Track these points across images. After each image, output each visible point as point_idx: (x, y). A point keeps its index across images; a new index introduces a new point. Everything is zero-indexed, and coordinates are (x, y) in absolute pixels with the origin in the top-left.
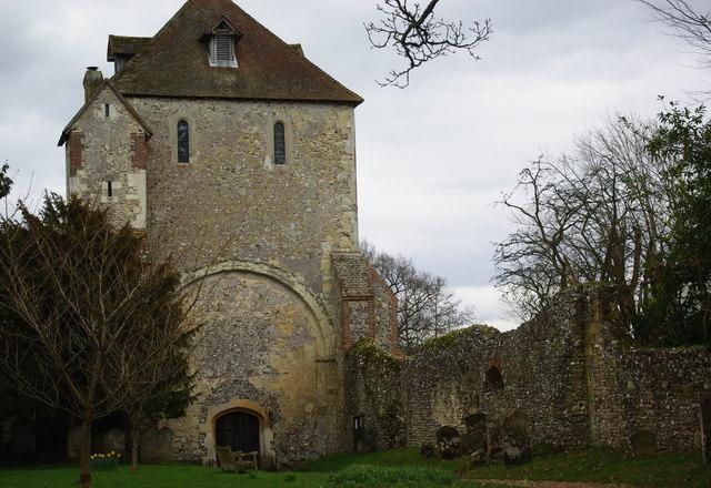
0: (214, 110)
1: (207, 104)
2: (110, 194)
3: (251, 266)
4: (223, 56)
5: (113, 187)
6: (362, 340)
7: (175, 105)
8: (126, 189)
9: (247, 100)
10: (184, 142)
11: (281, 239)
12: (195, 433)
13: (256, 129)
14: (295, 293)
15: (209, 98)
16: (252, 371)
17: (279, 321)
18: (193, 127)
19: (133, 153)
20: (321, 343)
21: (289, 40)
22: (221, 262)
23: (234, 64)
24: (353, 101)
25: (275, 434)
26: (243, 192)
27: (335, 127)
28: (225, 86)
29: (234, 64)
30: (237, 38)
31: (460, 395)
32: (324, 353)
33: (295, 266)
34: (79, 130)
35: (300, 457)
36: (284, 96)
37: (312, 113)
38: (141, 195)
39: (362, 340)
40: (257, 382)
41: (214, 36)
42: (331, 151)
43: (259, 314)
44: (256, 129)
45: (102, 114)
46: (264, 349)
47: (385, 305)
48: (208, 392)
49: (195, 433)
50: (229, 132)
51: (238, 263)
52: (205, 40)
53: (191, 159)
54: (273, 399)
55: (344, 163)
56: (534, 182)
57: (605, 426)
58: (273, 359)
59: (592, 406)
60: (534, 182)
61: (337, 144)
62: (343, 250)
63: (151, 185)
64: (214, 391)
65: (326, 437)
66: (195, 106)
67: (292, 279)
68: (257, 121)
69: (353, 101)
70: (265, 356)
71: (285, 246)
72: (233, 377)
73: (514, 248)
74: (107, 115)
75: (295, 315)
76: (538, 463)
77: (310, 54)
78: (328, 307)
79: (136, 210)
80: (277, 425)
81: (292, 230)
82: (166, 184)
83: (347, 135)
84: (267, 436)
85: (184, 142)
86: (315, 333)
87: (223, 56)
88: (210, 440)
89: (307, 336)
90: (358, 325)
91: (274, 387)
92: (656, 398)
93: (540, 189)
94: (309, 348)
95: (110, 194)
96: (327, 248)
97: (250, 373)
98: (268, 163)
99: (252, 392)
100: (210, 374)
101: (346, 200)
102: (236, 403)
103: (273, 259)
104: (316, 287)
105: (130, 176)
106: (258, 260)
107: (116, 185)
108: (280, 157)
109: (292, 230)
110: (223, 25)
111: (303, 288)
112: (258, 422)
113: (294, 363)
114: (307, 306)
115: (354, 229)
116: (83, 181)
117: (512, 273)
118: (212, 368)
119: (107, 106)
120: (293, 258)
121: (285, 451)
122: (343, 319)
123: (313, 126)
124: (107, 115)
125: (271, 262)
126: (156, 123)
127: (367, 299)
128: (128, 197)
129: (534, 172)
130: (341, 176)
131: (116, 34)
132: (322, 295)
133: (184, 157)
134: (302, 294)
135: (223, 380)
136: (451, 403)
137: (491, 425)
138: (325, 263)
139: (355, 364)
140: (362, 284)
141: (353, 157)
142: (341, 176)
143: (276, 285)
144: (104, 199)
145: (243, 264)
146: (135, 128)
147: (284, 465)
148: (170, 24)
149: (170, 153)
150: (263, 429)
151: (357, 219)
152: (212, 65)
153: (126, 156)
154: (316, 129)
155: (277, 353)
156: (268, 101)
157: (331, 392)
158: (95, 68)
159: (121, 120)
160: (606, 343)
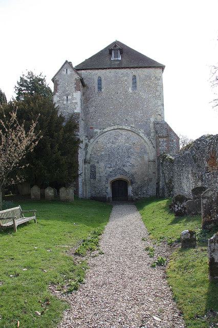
3: (124, 127)
4: (116, 56)
6: (164, 153)
7: (96, 71)
9: (122, 68)
11: (135, 117)
12: (104, 187)
13: (125, 78)
18: (103, 79)
20: (152, 155)
23: (120, 59)
29: (120, 59)
31: (194, 174)
32: (152, 158)
33: (141, 127)
34: (57, 79)
35: (142, 196)
39: (164, 153)
40: (126, 169)
42: (154, 85)
44: (125, 78)
45: (65, 73)
47: (174, 141)
55: (159, 88)
63: (86, 100)
64: (111, 172)
66: (104, 71)
67: (139, 131)
68: (126, 74)
69: (162, 67)
79: (76, 106)
81: (139, 114)
84: (130, 189)
88: (109, 190)
89: (145, 152)
90: (163, 147)
91: (133, 171)
96: (152, 120)
97: (124, 166)
98: (130, 90)
100: (109, 166)
102: (118, 177)
104: (148, 134)
107: (69, 97)
109: (139, 114)
110: (115, 46)
114: (145, 142)
116: (58, 96)
121: (137, 195)
122: (157, 146)
130: (157, 94)
133: (100, 88)
136: (189, 178)
137: (204, 201)
138: (152, 125)
141: (162, 87)
144: (65, 102)
146: (76, 76)
153: (73, 86)
154: (148, 77)
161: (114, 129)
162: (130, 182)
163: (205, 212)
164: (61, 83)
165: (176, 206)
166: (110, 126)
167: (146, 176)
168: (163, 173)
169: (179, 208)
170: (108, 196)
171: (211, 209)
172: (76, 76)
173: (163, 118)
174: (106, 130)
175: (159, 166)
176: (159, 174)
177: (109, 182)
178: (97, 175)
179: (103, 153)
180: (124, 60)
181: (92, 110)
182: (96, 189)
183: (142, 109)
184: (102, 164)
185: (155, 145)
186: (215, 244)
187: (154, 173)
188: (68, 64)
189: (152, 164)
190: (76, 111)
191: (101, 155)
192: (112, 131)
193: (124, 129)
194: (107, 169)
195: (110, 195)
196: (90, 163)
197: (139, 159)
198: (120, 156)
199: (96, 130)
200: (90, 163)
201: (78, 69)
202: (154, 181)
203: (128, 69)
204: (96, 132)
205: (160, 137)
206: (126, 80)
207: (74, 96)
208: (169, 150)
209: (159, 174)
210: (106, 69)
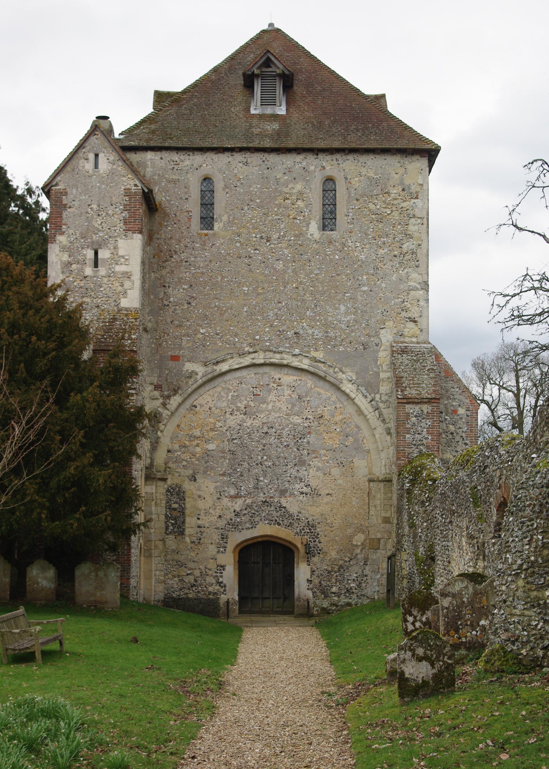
0: (246, 164)
1: (239, 156)
2: (96, 265)
3: (288, 359)
5: (100, 256)
7: (198, 158)
8: (116, 259)
10: (207, 205)
11: (326, 325)
12: (212, 565)
13: (299, 187)
14: (344, 392)
15: (241, 150)
16: (286, 491)
17: (322, 428)
18: (219, 186)
19: (125, 214)
20: (379, 458)
21: (368, 88)
22: (250, 353)
23: (282, 110)
25: (313, 572)
26: (280, 266)
27: (402, 183)
28: (262, 136)
29: (282, 110)
30: (288, 82)
32: (380, 471)
34: (61, 187)
35: (344, 600)
36: (336, 144)
37: (373, 165)
38: (134, 267)
40: (292, 505)
41: (257, 76)
42: (396, 214)
43: (297, 420)
44: (299, 187)
45: (89, 166)
46: (302, 463)
47: (461, 411)
48: (230, 515)
49: (212, 565)
50: (262, 192)
51: (271, 354)
52: (249, 82)
53: (216, 226)
54: (311, 526)
55: (412, 228)
58: (313, 476)
61: (404, 205)
62: (407, 339)
63: (157, 260)
64: (237, 514)
66: (223, 159)
67: (340, 375)
68: (301, 177)
69: (430, 153)
70: (303, 473)
71: (332, 334)
72: (261, 497)
74: (96, 166)
75: (343, 421)
78: (385, 412)
79: (127, 284)
80: (315, 559)
81: (341, 314)
82: (183, 256)
83: (419, 193)
84: (302, 573)
85: (207, 205)
86: (369, 445)
87: (268, 100)
88: (230, 575)
89: (358, 448)
91: (313, 511)
94: (361, 465)
95: (96, 265)
96: (387, 337)
97: (283, 493)
98: (314, 229)
99: (286, 517)
100: (233, 492)
101: (414, 275)
102: (264, 529)
103: (316, 350)
104: (370, 387)
105: (121, 243)
106: (297, 351)
107: (103, 254)
108: (328, 221)
109: (341, 314)
110: (268, 63)
111: (353, 388)
113: (340, 482)
114: (360, 412)
115: (424, 312)
116: (64, 249)
117: (407, 318)
118: (235, 485)
119: (97, 156)
120: (341, 348)
122: (400, 428)
123: (373, 182)
124: (96, 166)
125: (313, 354)
126: (174, 182)
127: (429, 401)
128: (119, 269)
132: (378, 397)
133: (207, 221)
134: (353, 395)
135: (249, 501)
136: (462, 549)
138: (384, 356)
141: (425, 220)
143: (321, 383)
144: (89, 271)
145: (278, 356)
146: (131, 183)
147: (323, 609)
148: (215, 70)
149: (189, 219)
150: (298, 564)
151: (427, 300)
152: (253, 112)
153: (117, 217)
154: (380, 186)
155: (318, 469)
156: (316, 151)
158: (106, 118)
159: (112, 173)
161: (254, 365)
162: (302, 550)
163: (447, 624)
164: (74, 198)
165: (410, 619)
166: (242, 354)
167: (361, 529)
168: (412, 526)
169: (418, 624)
170: (223, 598)
171: (460, 619)
172: (131, 183)
173: (424, 330)
174: (224, 367)
175: (400, 498)
176: (399, 526)
177: (231, 545)
178: (190, 522)
179: (211, 447)
180: (295, 115)
181: (177, 294)
182: (183, 571)
183: (353, 298)
184: (207, 486)
185: (392, 425)
186: (405, 652)
187: (386, 520)
188: (100, 127)
189: (379, 490)
190: (124, 303)
191: (207, 453)
192: (244, 373)
193: (287, 366)
194: (225, 501)
195: (232, 593)
196: (165, 480)
197: (336, 471)
198: (269, 458)
199: (189, 367)
200: (165, 480)
201: (130, 147)
202: (380, 557)
203: (311, 158)
204: (192, 374)
205: (409, 401)
206: (300, 195)
207: (121, 252)
208: (443, 438)
209: (399, 526)
210: (232, 150)
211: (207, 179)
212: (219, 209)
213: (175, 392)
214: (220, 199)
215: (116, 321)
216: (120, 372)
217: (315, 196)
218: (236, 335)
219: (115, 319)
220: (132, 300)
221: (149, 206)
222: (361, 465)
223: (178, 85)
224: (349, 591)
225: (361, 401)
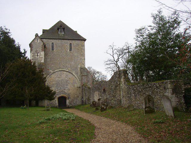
1: (57, 40)
3: (65, 70)
7: (51, 40)
8: (40, 55)
10: (53, 47)
15: (58, 39)
18: (54, 44)
20: (78, 84)
21: (75, 30)
24: (85, 40)
29: (63, 33)
30: (64, 29)
32: (78, 86)
37: (77, 42)
38: (43, 56)
43: (66, 79)
45: (36, 41)
50: (60, 45)
52: (58, 29)
56: (112, 48)
57: (125, 102)
58: (69, 87)
59: (122, 98)
60: (112, 48)
63: (46, 55)
65: (79, 102)
66: (55, 40)
69: (85, 40)
73: (109, 62)
76: (110, 111)
77: (78, 33)
79: (42, 59)
83: (84, 46)
84: (68, 101)
85: (53, 47)
90: (85, 80)
92: (135, 96)
93: (113, 50)
94: (76, 85)
96: (79, 66)
98: (69, 50)
100: (57, 90)
102: (62, 95)
104: (77, 74)
107: (38, 54)
108: (71, 50)
112: (66, 99)
122: (81, 80)
128: (41, 56)
129: (112, 46)
131: (45, 29)
133: (53, 49)
138: (79, 69)
139: (83, 88)
140: (85, 73)
141: (84, 50)
142: (82, 53)
144: (36, 57)
153: (41, 49)
157: (80, 93)
160: (125, 83)
167: (76, 94)
179: (54, 83)
181: (48, 60)
188: (37, 35)
190: (42, 62)
191: (53, 84)
199: (50, 71)
201: (41, 38)
203: (68, 40)
204: (51, 72)
211: (53, 43)
212: (55, 48)
213: (48, 75)
214: (55, 46)
215: (41, 65)
216: (41, 71)
217: (69, 46)
218: (57, 66)
219: (40, 64)
220: (43, 61)
221: (45, 47)
222: (76, 85)
223: (48, 28)
224: (74, 104)
225: (75, 76)
